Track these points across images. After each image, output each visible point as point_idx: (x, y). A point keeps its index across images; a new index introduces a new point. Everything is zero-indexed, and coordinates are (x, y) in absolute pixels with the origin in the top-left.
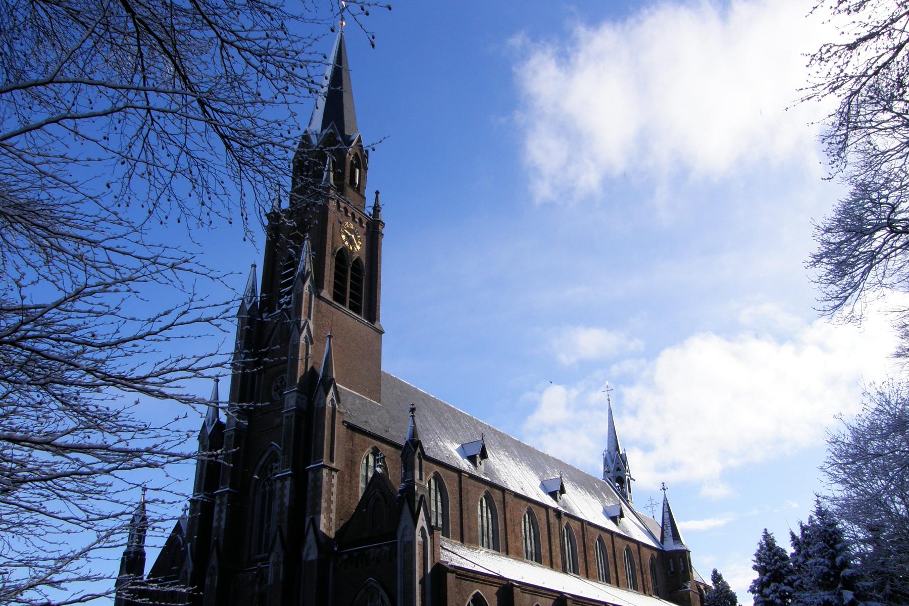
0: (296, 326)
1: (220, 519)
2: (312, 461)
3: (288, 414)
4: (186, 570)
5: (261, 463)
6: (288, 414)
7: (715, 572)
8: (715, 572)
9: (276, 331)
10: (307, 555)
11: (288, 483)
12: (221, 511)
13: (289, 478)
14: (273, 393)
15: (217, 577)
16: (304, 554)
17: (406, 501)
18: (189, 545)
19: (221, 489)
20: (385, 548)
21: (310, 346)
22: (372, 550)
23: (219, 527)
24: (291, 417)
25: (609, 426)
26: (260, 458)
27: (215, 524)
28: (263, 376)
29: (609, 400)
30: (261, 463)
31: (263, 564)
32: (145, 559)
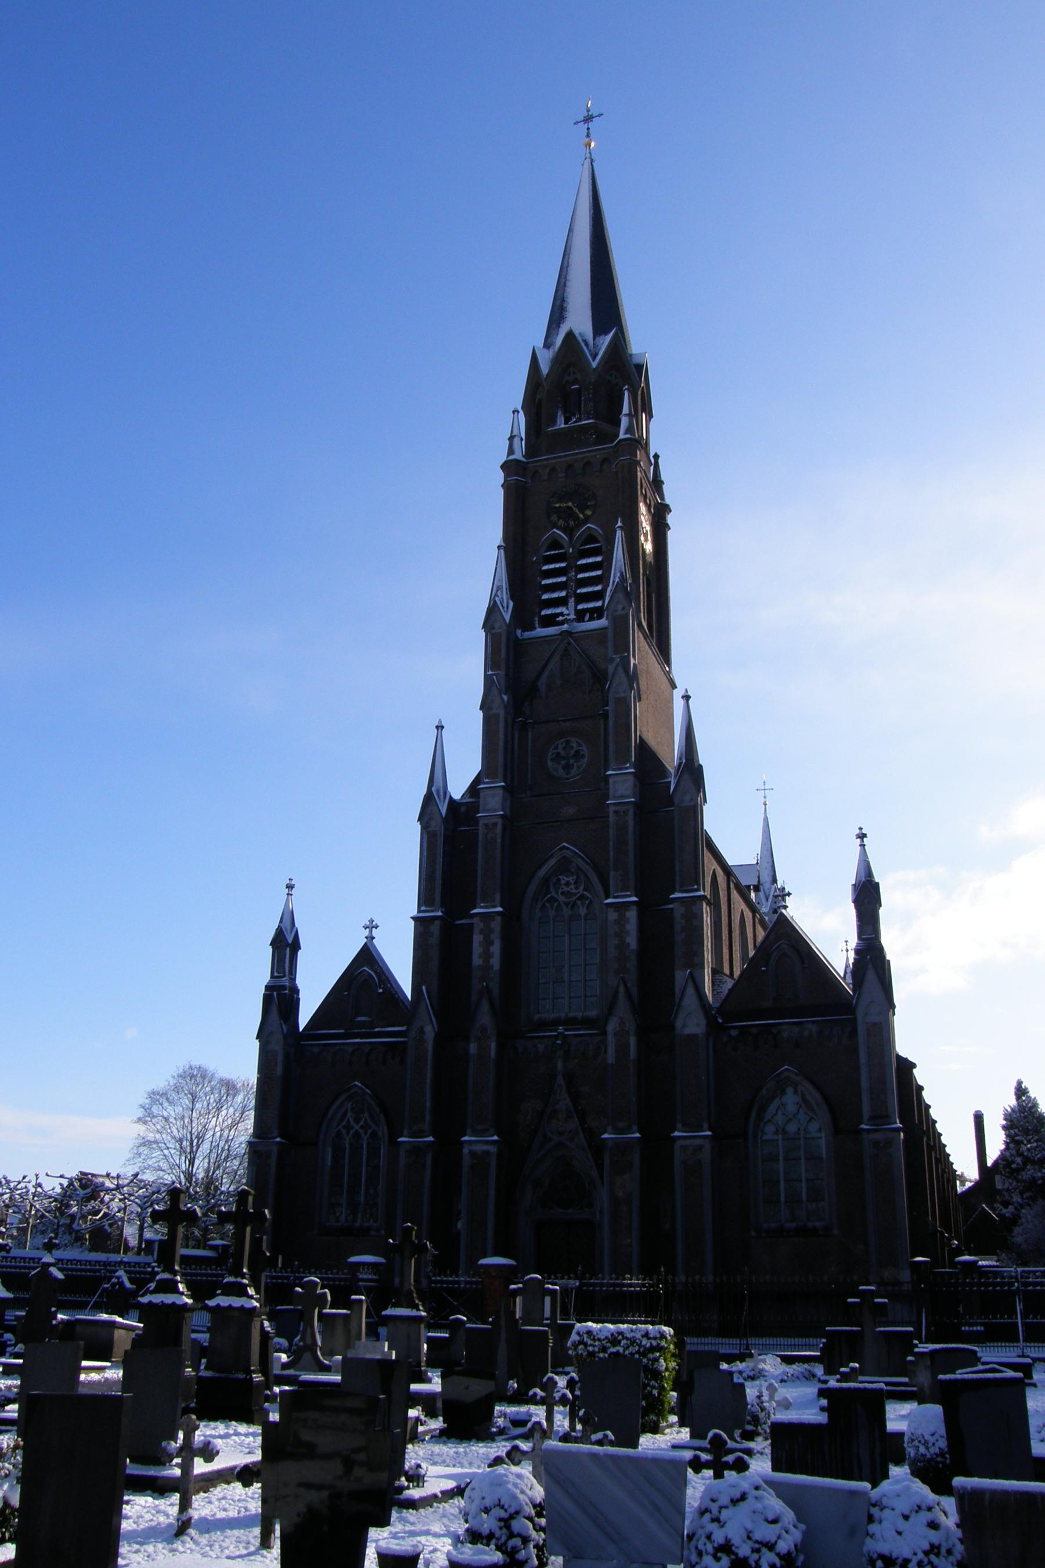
0: (620, 670)
1: (487, 955)
2: (677, 886)
3: (618, 808)
4: (422, 1027)
5: (542, 872)
6: (618, 808)
7: (1020, 1083)
8: (1020, 1083)
9: (551, 666)
10: (684, 1026)
11: (632, 914)
12: (488, 943)
13: (635, 908)
14: (550, 763)
15: (493, 1045)
16: (678, 1024)
17: (870, 966)
18: (424, 988)
19: (481, 907)
20: (810, 1026)
21: (638, 704)
22: (784, 1027)
23: (486, 967)
24: (625, 813)
25: (763, 844)
26: (541, 866)
27: (477, 961)
28: (530, 733)
29: (765, 804)
30: (542, 872)
31: (566, 1030)
32: (298, 1000)
